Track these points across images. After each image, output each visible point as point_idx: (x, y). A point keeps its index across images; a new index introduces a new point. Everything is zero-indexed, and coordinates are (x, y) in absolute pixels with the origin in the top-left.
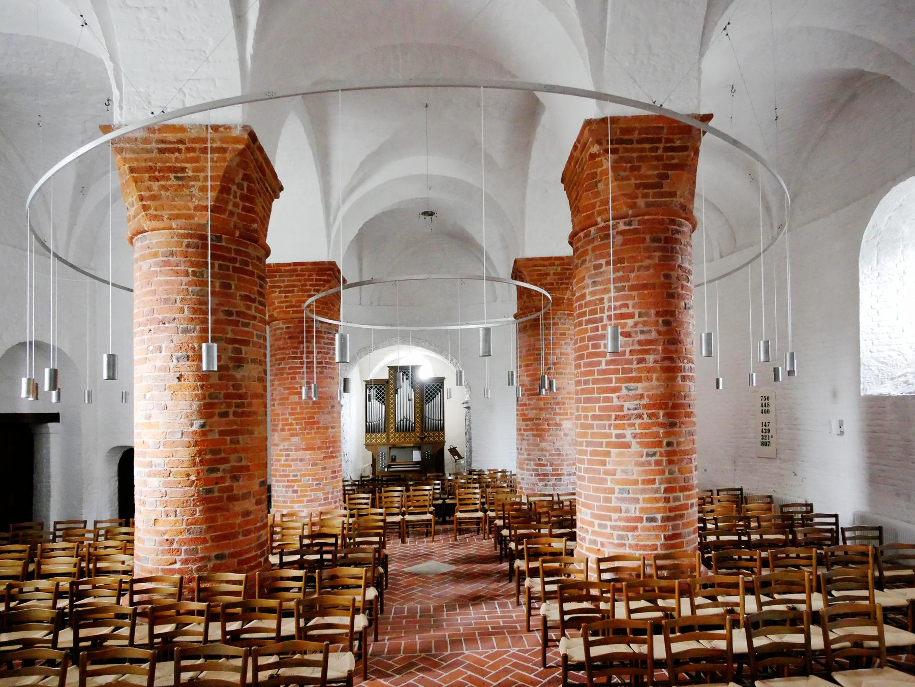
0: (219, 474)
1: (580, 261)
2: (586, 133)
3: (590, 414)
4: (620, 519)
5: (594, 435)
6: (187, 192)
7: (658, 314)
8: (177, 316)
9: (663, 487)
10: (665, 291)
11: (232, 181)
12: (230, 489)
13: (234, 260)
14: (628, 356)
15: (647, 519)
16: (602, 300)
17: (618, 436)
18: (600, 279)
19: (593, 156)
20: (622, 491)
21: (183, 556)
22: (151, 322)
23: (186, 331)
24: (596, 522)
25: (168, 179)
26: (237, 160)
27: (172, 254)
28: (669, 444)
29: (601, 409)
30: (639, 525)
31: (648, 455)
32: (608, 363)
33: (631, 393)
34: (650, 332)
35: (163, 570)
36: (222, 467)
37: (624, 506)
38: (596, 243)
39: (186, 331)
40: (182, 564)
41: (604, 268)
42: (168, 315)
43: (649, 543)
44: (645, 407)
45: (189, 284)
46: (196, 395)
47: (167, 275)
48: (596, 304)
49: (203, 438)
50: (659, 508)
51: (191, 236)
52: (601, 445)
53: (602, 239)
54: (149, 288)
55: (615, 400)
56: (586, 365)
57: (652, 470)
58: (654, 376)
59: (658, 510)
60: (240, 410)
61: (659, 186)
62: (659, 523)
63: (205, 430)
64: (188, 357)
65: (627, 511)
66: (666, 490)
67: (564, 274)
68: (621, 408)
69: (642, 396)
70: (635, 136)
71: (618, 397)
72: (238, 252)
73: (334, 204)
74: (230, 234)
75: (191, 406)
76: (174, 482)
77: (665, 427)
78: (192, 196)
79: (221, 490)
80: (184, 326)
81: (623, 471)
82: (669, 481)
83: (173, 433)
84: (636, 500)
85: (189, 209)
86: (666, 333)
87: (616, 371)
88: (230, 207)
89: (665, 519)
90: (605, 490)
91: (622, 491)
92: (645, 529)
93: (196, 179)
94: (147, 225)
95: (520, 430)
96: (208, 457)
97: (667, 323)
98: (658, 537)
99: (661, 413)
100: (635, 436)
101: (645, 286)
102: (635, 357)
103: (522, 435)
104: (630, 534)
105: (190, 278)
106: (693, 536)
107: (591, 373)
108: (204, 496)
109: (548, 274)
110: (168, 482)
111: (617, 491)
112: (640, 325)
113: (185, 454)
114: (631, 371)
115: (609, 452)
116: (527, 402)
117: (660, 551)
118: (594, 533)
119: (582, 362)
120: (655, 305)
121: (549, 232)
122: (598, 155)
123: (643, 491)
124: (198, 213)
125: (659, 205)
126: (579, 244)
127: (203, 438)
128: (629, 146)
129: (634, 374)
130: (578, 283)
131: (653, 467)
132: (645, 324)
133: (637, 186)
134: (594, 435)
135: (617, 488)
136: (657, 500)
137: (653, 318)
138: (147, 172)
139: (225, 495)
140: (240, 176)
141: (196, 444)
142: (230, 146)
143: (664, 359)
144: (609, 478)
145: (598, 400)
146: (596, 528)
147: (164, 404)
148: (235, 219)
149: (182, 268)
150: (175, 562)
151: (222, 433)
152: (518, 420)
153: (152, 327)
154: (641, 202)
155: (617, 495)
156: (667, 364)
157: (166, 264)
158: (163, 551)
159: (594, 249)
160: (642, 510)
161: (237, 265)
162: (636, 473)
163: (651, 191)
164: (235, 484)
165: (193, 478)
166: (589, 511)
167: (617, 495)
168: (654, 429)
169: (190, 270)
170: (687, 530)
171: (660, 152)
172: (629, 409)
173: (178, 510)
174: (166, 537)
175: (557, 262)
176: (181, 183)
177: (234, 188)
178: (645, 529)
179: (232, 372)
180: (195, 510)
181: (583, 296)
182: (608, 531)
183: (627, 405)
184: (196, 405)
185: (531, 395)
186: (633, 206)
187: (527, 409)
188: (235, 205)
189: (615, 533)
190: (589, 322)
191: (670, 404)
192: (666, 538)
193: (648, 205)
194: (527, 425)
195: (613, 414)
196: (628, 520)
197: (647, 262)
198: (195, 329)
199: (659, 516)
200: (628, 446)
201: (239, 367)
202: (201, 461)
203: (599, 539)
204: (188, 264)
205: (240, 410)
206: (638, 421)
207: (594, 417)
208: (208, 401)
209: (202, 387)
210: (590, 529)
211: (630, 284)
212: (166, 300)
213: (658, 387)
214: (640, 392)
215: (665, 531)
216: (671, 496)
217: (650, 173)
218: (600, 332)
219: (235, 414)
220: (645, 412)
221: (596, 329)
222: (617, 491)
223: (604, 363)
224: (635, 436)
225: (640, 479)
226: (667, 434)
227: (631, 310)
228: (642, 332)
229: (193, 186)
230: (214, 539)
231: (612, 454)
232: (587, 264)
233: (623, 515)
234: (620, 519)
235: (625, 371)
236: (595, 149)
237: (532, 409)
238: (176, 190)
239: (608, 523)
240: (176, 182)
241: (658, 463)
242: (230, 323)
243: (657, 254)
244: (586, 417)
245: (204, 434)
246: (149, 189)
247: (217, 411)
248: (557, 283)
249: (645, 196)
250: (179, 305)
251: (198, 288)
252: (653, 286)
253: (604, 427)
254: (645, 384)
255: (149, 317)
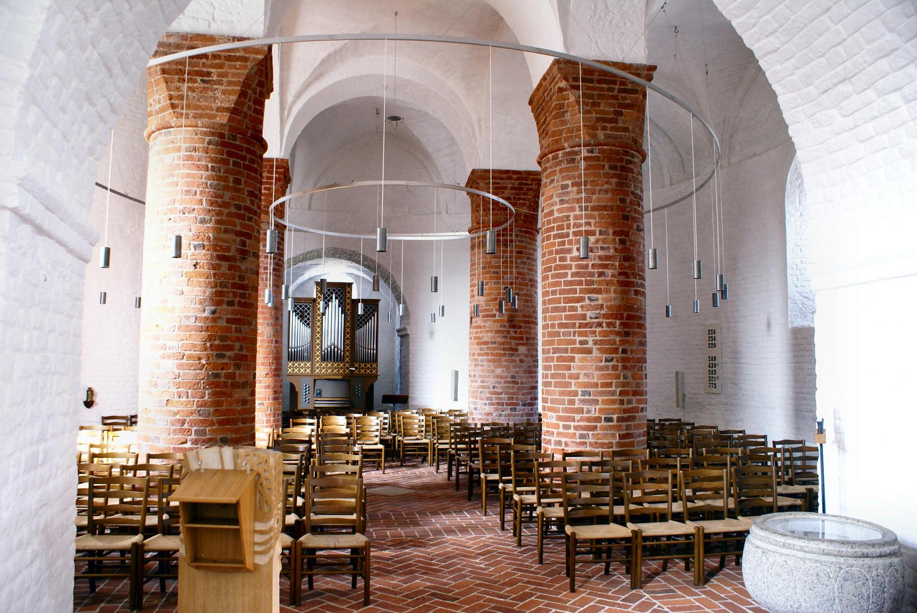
0: (226, 361)
1: (548, 181)
2: (556, 68)
3: (557, 322)
4: (582, 420)
5: (560, 342)
6: (210, 94)
7: (615, 233)
8: (196, 207)
9: (618, 390)
10: (621, 213)
11: (249, 86)
12: (232, 376)
13: (244, 158)
14: (590, 269)
15: (605, 418)
16: (568, 217)
17: (581, 343)
18: (567, 198)
19: (561, 90)
20: (584, 393)
21: (193, 436)
22: (171, 211)
23: (203, 221)
24: (561, 424)
25: (195, 81)
26: (256, 68)
27: (195, 150)
28: (624, 351)
29: (567, 317)
30: (598, 425)
31: (606, 361)
32: (573, 275)
33: (593, 303)
34: (608, 248)
35: (174, 448)
36: (228, 353)
37: (585, 407)
38: (563, 166)
39: (203, 221)
40: (193, 443)
41: (570, 189)
42: (188, 206)
43: (606, 441)
44: (604, 316)
45: (208, 178)
46: (209, 283)
47: (189, 168)
48: (563, 221)
49: (214, 324)
50: (615, 409)
51: (213, 134)
52: (566, 351)
53: (569, 162)
54: (172, 180)
55: (579, 309)
56: (553, 276)
57: (609, 374)
58: (612, 288)
59: (614, 411)
60: (243, 301)
61: (614, 121)
62: (615, 423)
63: (215, 316)
64: (204, 246)
65: (589, 411)
66: (621, 393)
67: (521, 189)
68: (584, 317)
69: (602, 307)
70: (595, 77)
71: (582, 307)
72: (249, 151)
73: (290, 98)
74: (244, 134)
75: (204, 292)
76: (187, 364)
77: (621, 336)
78: (215, 98)
79: (228, 376)
80: (202, 216)
81: (585, 375)
82: (623, 385)
83: (188, 317)
84: (596, 402)
85: (212, 109)
86: (622, 251)
87: (580, 283)
88: (245, 109)
89: (620, 420)
90: (569, 393)
91: (584, 393)
92: (603, 428)
93: (219, 83)
94: (173, 121)
95: (474, 354)
96: (217, 342)
97: (622, 242)
98: (613, 435)
99: (618, 322)
100: (595, 343)
101: (604, 208)
102: (596, 271)
103: (476, 360)
104: (590, 433)
105: (209, 173)
106: (642, 438)
107: (558, 284)
108: (212, 380)
109: (506, 188)
110: (182, 364)
111: (580, 393)
112: (600, 242)
113: (197, 339)
114: (592, 283)
115: (574, 357)
116: (482, 324)
117: (615, 449)
118: (559, 434)
119: (550, 273)
120: (613, 225)
121: (513, 144)
122: (566, 90)
123: (602, 394)
124: (219, 114)
125: (615, 138)
126: (548, 165)
127: (214, 324)
128: (591, 85)
129: (595, 286)
130: (546, 200)
131: (610, 372)
132: (604, 241)
133: (598, 119)
134: (560, 342)
135: (580, 390)
136: (613, 402)
137: (611, 237)
138: (177, 74)
139: (230, 381)
140: (256, 82)
141: (207, 329)
142: (252, 56)
143: (620, 274)
144: (573, 381)
145: (564, 309)
146: (561, 430)
147: (180, 289)
148: (247, 120)
149: (203, 163)
150: (186, 442)
151: (229, 321)
152: (471, 344)
153: (172, 217)
154: (601, 135)
155: (580, 397)
156: (622, 278)
157: (189, 158)
158: (174, 431)
159: (561, 171)
160: (601, 410)
161: (247, 163)
162: (596, 377)
163: (609, 125)
164: (237, 372)
165: (203, 361)
166: (554, 415)
167: (580, 397)
168: (612, 337)
169: (210, 166)
170: (637, 432)
171: (615, 92)
172: (591, 318)
173: (190, 391)
174: (178, 417)
175: (515, 176)
176: (206, 86)
177: (250, 92)
178: (603, 428)
179: (238, 264)
180: (204, 393)
181: (551, 213)
182: (572, 431)
183: (589, 314)
184: (209, 291)
185: (488, 316)
186: (594, 136)
187: (481, 332)
188: (249, 107)
189: (578, 433)
190: (556, 237)
191: (625, 315)
192: (621, 437)
193: (606, 136)
194: (481, 349)
195: (578, 322)
196: (589, 420)
197: (606, 187)
198: (211, 220)
199: (615, 417)
200: (590, 351)
201: (244, 258)
202: (211, 346)
203: (563, 440)
204: (208, 159)
205: (243, 301)
206: (598, 329)
207: (561, 325)
208: (219, 289)
209: (215, 275)
210: (555, 431)
211: (592, 204)
212: (188, 192)
213: (615, 298)
214: (600, 302)
215: (619, 430)
216: (625, 398)
217: (607, 109)
218: (567, 246)
219: (239, 303)
220: (604, 321)
221: (563, 243)
222: (580, 393)
223: (569, 275)
224: (595, 343)
225: (599, 382)
226: (622, 342)
227: (593, 228)
228: (602, 248)
229: (216, 89)
230: (221, 423)
231: (576, 359)
232: (555, 184)
233: (585, 415)
234: (582, 420)
235: (588, 283)
236: (563, 84)
237: (487, 332)
238: (201, 92)
239: (572, 424)
240: (202, 85)
241: (615, 368)
242: (242, 217)
243: (614, 180)
244: (553, 326)
245: (215, 320)
246: (178, 89)
247: (226, 299)
248: (515, 198)
249: (604, 128)
250: (198, 197)
251: (216, 182)
252: (611, 208)
253: (569, 334)
254: (604, 296)
255: (169, 207)
